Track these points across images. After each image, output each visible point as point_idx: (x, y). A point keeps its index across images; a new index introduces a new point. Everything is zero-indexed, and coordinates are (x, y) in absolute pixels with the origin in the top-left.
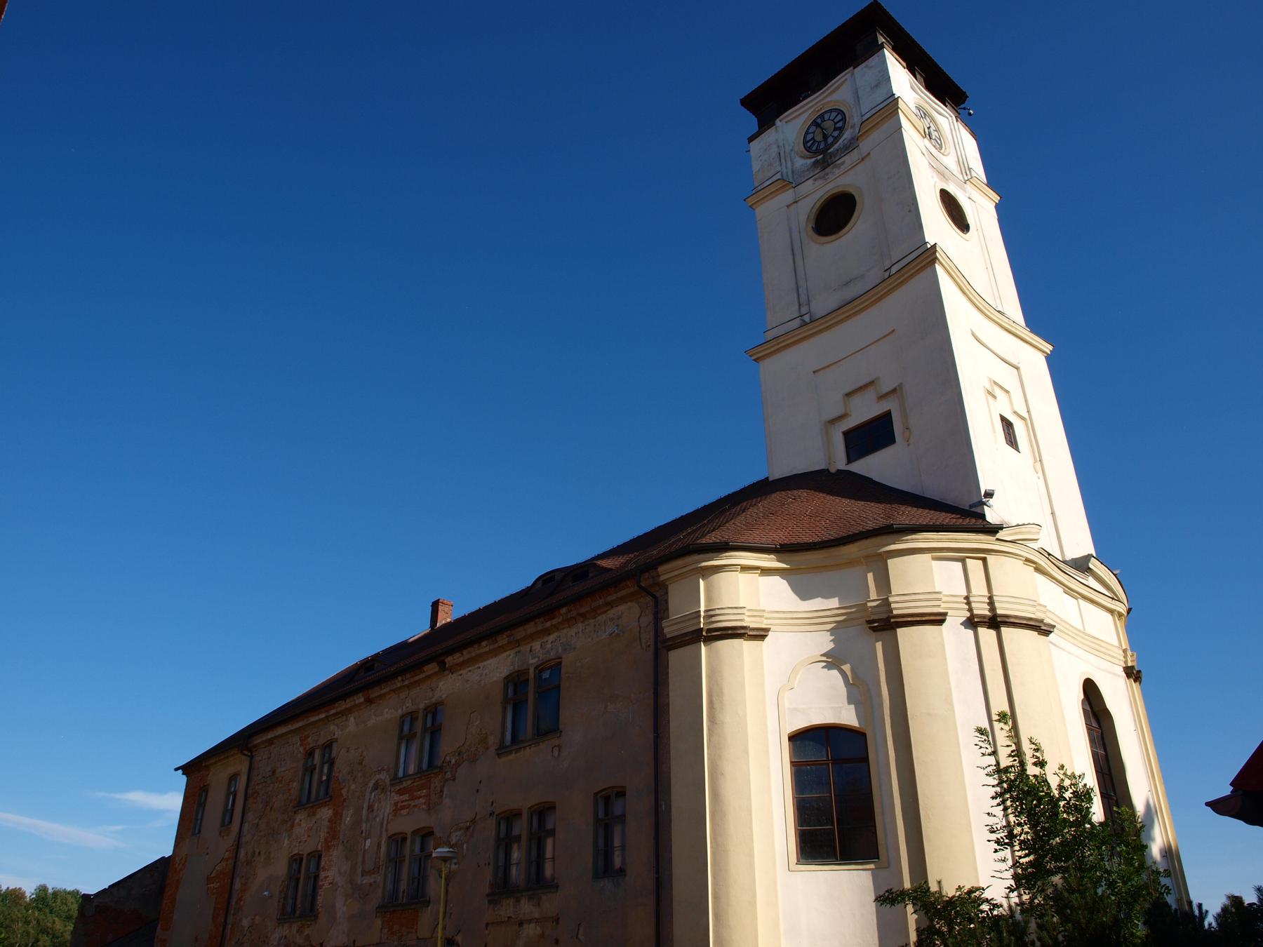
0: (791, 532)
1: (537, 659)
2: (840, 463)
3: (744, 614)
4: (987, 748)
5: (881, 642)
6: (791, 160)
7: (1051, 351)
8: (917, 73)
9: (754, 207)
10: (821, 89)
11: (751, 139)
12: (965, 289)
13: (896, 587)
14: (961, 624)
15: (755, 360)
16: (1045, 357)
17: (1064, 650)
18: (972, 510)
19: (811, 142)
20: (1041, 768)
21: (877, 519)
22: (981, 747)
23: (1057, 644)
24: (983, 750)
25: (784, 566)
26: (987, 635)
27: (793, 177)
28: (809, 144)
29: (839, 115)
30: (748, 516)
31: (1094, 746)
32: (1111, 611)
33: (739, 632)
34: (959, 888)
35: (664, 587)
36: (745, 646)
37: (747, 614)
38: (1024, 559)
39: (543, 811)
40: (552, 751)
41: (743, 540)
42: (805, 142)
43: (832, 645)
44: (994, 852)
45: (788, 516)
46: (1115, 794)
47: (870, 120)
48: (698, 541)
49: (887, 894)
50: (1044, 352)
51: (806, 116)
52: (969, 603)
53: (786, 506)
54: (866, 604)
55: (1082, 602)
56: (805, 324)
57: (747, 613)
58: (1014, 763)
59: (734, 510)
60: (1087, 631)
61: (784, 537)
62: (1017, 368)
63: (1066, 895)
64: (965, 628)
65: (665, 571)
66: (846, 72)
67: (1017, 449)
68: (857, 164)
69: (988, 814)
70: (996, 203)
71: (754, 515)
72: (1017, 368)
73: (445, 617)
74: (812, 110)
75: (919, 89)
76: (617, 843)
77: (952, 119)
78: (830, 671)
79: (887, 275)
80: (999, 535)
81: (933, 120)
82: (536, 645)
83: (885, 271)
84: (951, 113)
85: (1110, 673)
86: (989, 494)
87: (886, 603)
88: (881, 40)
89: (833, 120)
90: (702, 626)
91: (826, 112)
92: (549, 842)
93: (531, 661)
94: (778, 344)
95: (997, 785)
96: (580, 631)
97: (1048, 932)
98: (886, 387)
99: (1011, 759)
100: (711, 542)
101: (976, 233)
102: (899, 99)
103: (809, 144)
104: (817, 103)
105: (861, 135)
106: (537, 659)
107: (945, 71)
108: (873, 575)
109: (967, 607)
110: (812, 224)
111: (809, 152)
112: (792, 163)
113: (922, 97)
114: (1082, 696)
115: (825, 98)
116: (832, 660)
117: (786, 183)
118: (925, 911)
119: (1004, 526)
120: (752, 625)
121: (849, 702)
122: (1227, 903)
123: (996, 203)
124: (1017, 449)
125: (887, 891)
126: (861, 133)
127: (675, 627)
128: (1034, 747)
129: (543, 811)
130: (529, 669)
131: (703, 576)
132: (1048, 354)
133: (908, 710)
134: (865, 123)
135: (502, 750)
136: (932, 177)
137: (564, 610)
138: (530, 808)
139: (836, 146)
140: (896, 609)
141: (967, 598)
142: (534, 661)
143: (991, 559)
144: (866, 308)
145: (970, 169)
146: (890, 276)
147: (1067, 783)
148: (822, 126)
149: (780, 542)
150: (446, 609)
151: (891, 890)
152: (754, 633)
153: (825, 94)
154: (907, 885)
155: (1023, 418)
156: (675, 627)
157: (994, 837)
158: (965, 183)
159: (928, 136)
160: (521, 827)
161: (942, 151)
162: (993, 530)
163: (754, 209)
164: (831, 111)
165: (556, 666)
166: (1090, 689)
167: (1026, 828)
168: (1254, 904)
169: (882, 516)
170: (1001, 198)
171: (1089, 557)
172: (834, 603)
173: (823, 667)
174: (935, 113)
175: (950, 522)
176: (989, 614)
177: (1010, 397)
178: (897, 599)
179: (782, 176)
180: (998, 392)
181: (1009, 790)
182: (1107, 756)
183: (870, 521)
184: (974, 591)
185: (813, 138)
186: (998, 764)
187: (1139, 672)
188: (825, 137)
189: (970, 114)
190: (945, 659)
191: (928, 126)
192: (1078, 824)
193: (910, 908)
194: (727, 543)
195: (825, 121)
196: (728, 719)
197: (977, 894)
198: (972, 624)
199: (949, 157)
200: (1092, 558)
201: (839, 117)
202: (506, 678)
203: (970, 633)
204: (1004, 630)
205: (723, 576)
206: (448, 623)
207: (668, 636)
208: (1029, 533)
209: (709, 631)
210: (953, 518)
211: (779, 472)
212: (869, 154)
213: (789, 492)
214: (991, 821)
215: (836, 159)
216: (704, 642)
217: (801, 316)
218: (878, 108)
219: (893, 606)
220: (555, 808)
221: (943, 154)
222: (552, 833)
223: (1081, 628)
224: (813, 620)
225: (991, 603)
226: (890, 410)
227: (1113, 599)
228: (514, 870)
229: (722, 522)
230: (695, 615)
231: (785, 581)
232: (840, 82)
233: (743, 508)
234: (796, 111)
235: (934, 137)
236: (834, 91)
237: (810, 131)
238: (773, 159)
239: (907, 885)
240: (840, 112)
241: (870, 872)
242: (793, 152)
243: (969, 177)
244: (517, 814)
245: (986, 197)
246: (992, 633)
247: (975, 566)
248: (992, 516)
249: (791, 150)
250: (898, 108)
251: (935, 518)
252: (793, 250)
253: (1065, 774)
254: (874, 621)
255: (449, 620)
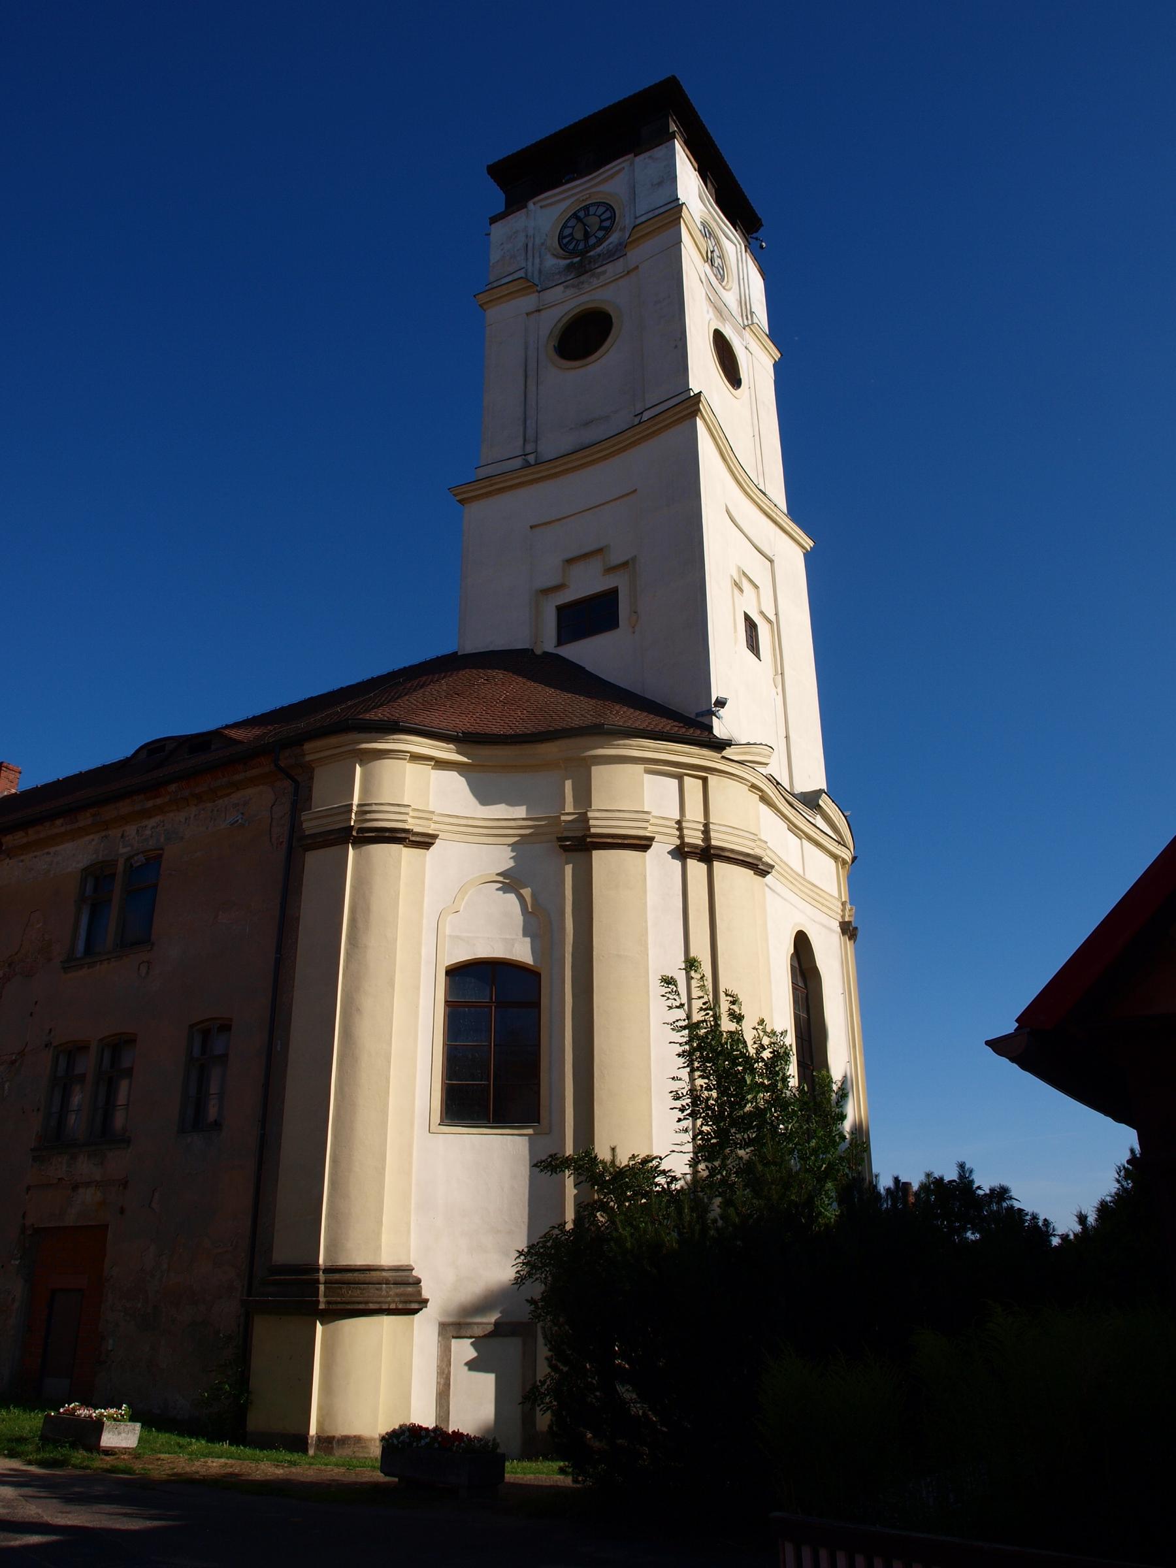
0: (478, 719)
1: (129, 848)
2: (548, 643)
3: (407, 814)
4: (675, 1000)
5: (571, 865)
6: (540, 257)
7: (811, 547)
8: (708, 181)
9: (485, 307)
10: (590, 174)
11: (494, 220)
12: (726, 454)
13: (599, 800)
14: (669, 853)
15: (459, 501)
16: (804, 554)
17: (778, 895)
18: (699, 719)
19: (568, 239)
20: (738, 1023)
21: (585, 717)
22: (668, 998)
23: (773, 888)
24: (669, 1003)
25: (465, 760)
26: (697, 868)
27: (539, 279)
28: (565, 241)
29: (608, 212)
30: (427, 693)
31: (797, 1009)
32: (835, 857)
33: (399, 835)
34: (634, 1157)
35: (309, 770)
36: (406, 855)
37: (411, 814)
38: (750, 784)
39: (119, 1045)
40: (139, 969)
41: (417, 721)
42: (561, 237)
43: (511, 864)
44: (678, 1121)
45: (477, 700)
46: (812, 1063)
47: (644, 225)
48: (361, 716)
49: (549, 1160)
50: (803, 547)
51: (571, 202)
52: (680, 829)
53: (476, 687)
54: (559, 817)
55: (807, 844)
56: (528, 465)
57: (411, 814)
58: (706, 1017)
59: (410, 685)
60: (808, 877)
61: (468, 724)
62: (771, 561)
63: (760, 1167)
64: (672, 858)
65: (313, 750)
66: (623, 159)
67: (757, 655)
68: (621, 277)
69: (673, 1078)
70: (775, 361)
71: (435, 693)
72: (771, 561)
73: (8, 787)
74: (576, 198)
75: (709, 201)
76: (214, 1089)
77: (741, 248)
78: (505, 895)
79: (636, 421)
80: (726, 753)
81: (718, 243)
82: (131, 830)
83: (635, 416)
84: (740, 240)
85: (824, 926)
86: (721, 703)
87: (583, 819)
88: (673, 127)
89: (599, 217)
90: (352, 824)
91: (592, 205)
92: (124, 1085)
93: (122, 850)
94: (491, 485)
95: (686, 1043)
96: (192, 816)
97: (736, 1209)
98: (616, 558)
99: (703, 1013)
100: (377, 718)
101: (748, 390)
102: (684, 207)
103: (565, 241)
104: (583, 190)
105: (631, 242)
106: (129, 848)
107: (744, 190)
108: (572, 782)
109: (678, 833)
110: (554, 342)
111: (564, 250)
112: (541, 261)
113: (710, 212)
114: (792, 951)
115: (595, 185)
116: (510, 882)
117: (529, 284)
118: (590, 1183)
119: (733, 743)
120: (417, 829)
121: (525, 934)
122: (924, 1181)
123: (775, 361)
124: (757, 655)
125: (551, 1156)
126: (630, 239)
127: (315, 823)
128: (730, 999)
129: (119, 1045)
130: (117, 861)
131: (361, 760)
132: (807, 551)
133: (595, 949)
134: (639, 228)
135: (70, 963)
136: (708, 312)
137: (173, 787)
138: (101, 1040)
139: (599, 249)
140: (595, 826)
141: (679, 822)
142: (125, 850)
143: (713, 780)
144: (605, 458)
145: (752, 313)
146: (640, 423)
147: (766, 1041)
148: (585, 220)
149: (463, 729)
150: (12, 776)
151: (555, 1154)
152: (418, 839)
153: (593, 183)
154: (569, 1151)
155: (770, 621)
156: (315, 823)
157: (678, 1104)
158: (744, 329)
159: (709, 261)
160: (87, 1065)
161: (724, 284)
162: (720, 745)
163: (485, 311)
164: (598, 204)
165: (154, 859)
166: (802, 943)
167: (714, 1094)
168: (954, 1181)
169: (591, 713)
170: (782, 355)
171: (819, 792)
172: (520, 812)
173: (498, 889)
174: (721, 233)
175: (671, 729)
176: (702, 844)
177: (758, 592)
178: (597, 814)
179: (526, 274)
180: (746, 585)
181: (699, 1048)
182: (809, 1019)
183: (577, 717)
184: (689, 815)
185: (571, 234)
186: (689, 1017)
187: (856, 929)
188: (587, 236)
189: (761, 247)
190: (645, 892)
191: (712, 249)
192: (772, 1088)
193: (570, 1182)
194: (396, 723)
195: (589, 215)
196: (373, 942)
197: (654, 1163)
198: (681, 854)
199: (730, 293)
200: (824, 794)
201: (608, 214)
202: (85, 870)
203: (677, 864)
204: (718, 866)
205: (387, 762)
206: (13, 794)
207: (307, 833)
208: (759, 754)
209: (361, 830)
210: (674, 726)
211: (472, 645)
212: (637, 267)
213: (482, 671)
214: (676, 1085)
215: (596, 266)
216: (353, 844)
217: (525, 455)
218: (657, 212)
219: (592, 822)
220: (135, 1041)
221: (724, 288)
222: (129, 1072)
223: (801, 873)
224: (493, 831)
225: (706, 831)
226: (617, 587)
227: (839, 843)
228: (72, 1118)
229: (392, 697)
230: (343, 809)
231: (463, 779)
232: (614, 170)
233: (421, 683)
234: (554, 195)
235: (716, 265)
236: (606, 180)
237: (568, 225)
238: (518, 250)
239: (569, 1151)
240: (609, 208)
241: (527, 1138)
242: (544, 247)
243: (750, 322)
244: (82, 1047)
245: (766, 352)
246: (703, 867)
247: (693, 786)
248: (720, 729)
249: (543, 244)
250: (681, 216)
251: (654, 723)
252: (526, 371)
253: (765, 1032)
254: (567, 839)
255: (13, 791)
